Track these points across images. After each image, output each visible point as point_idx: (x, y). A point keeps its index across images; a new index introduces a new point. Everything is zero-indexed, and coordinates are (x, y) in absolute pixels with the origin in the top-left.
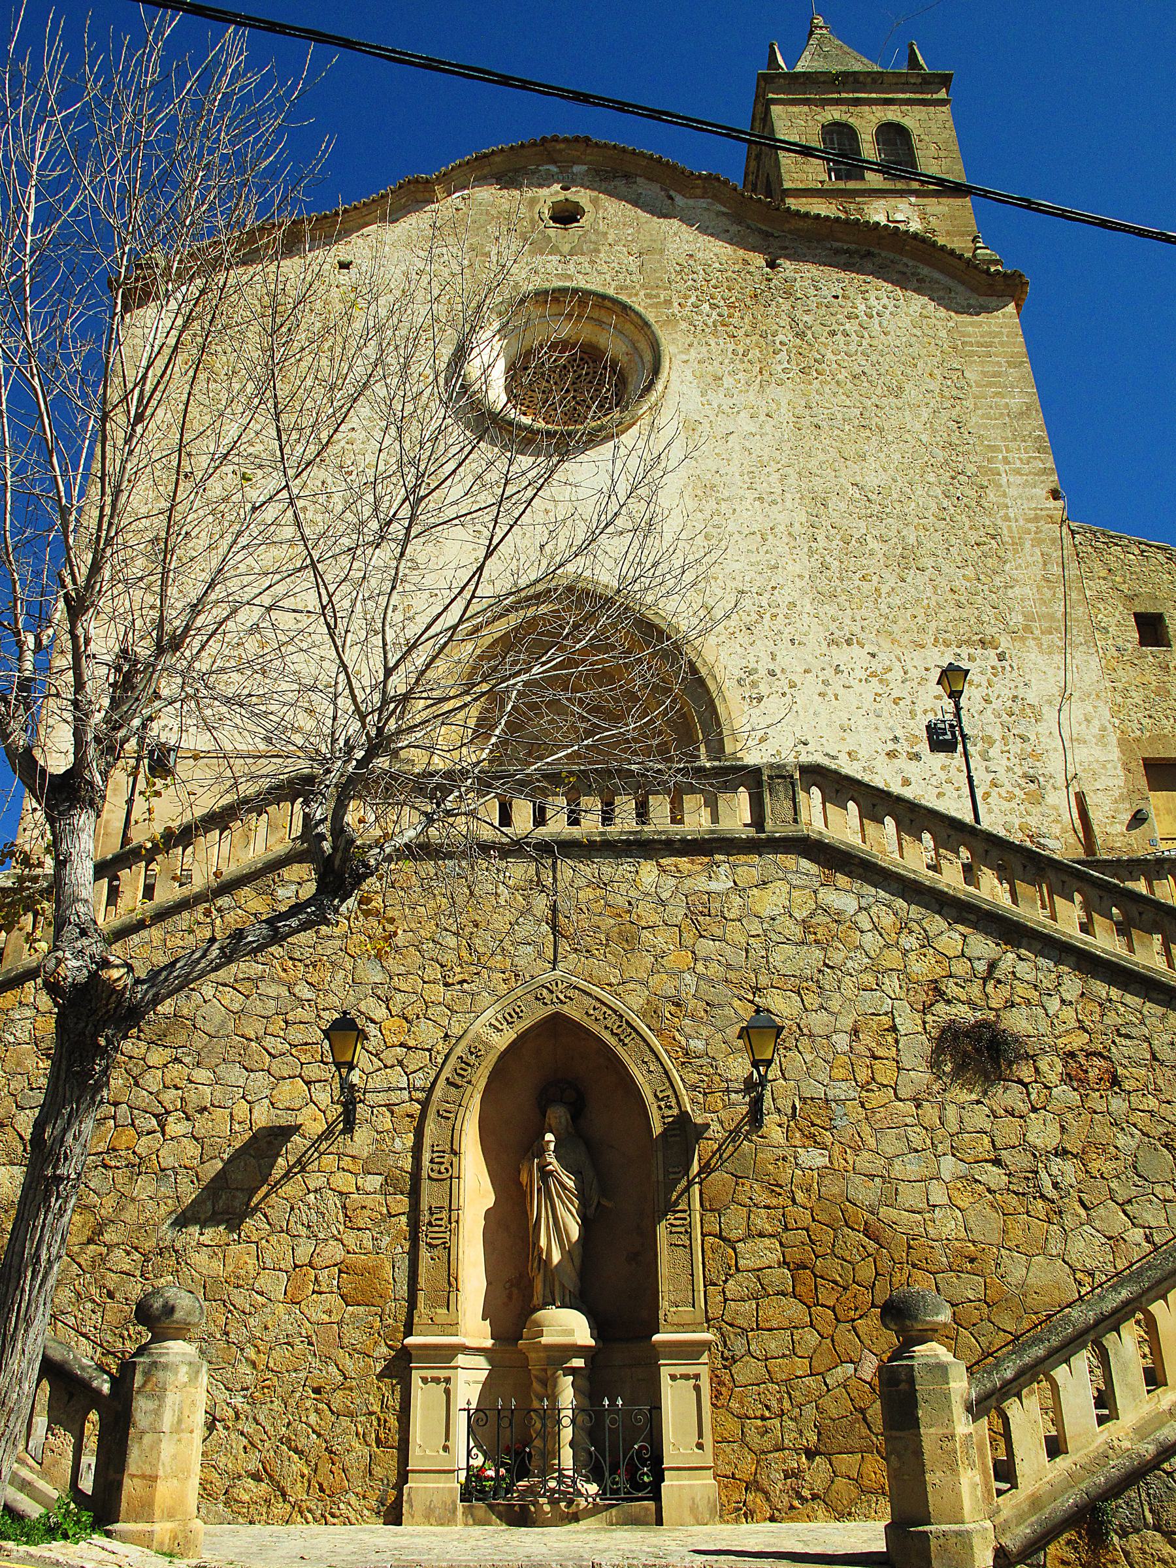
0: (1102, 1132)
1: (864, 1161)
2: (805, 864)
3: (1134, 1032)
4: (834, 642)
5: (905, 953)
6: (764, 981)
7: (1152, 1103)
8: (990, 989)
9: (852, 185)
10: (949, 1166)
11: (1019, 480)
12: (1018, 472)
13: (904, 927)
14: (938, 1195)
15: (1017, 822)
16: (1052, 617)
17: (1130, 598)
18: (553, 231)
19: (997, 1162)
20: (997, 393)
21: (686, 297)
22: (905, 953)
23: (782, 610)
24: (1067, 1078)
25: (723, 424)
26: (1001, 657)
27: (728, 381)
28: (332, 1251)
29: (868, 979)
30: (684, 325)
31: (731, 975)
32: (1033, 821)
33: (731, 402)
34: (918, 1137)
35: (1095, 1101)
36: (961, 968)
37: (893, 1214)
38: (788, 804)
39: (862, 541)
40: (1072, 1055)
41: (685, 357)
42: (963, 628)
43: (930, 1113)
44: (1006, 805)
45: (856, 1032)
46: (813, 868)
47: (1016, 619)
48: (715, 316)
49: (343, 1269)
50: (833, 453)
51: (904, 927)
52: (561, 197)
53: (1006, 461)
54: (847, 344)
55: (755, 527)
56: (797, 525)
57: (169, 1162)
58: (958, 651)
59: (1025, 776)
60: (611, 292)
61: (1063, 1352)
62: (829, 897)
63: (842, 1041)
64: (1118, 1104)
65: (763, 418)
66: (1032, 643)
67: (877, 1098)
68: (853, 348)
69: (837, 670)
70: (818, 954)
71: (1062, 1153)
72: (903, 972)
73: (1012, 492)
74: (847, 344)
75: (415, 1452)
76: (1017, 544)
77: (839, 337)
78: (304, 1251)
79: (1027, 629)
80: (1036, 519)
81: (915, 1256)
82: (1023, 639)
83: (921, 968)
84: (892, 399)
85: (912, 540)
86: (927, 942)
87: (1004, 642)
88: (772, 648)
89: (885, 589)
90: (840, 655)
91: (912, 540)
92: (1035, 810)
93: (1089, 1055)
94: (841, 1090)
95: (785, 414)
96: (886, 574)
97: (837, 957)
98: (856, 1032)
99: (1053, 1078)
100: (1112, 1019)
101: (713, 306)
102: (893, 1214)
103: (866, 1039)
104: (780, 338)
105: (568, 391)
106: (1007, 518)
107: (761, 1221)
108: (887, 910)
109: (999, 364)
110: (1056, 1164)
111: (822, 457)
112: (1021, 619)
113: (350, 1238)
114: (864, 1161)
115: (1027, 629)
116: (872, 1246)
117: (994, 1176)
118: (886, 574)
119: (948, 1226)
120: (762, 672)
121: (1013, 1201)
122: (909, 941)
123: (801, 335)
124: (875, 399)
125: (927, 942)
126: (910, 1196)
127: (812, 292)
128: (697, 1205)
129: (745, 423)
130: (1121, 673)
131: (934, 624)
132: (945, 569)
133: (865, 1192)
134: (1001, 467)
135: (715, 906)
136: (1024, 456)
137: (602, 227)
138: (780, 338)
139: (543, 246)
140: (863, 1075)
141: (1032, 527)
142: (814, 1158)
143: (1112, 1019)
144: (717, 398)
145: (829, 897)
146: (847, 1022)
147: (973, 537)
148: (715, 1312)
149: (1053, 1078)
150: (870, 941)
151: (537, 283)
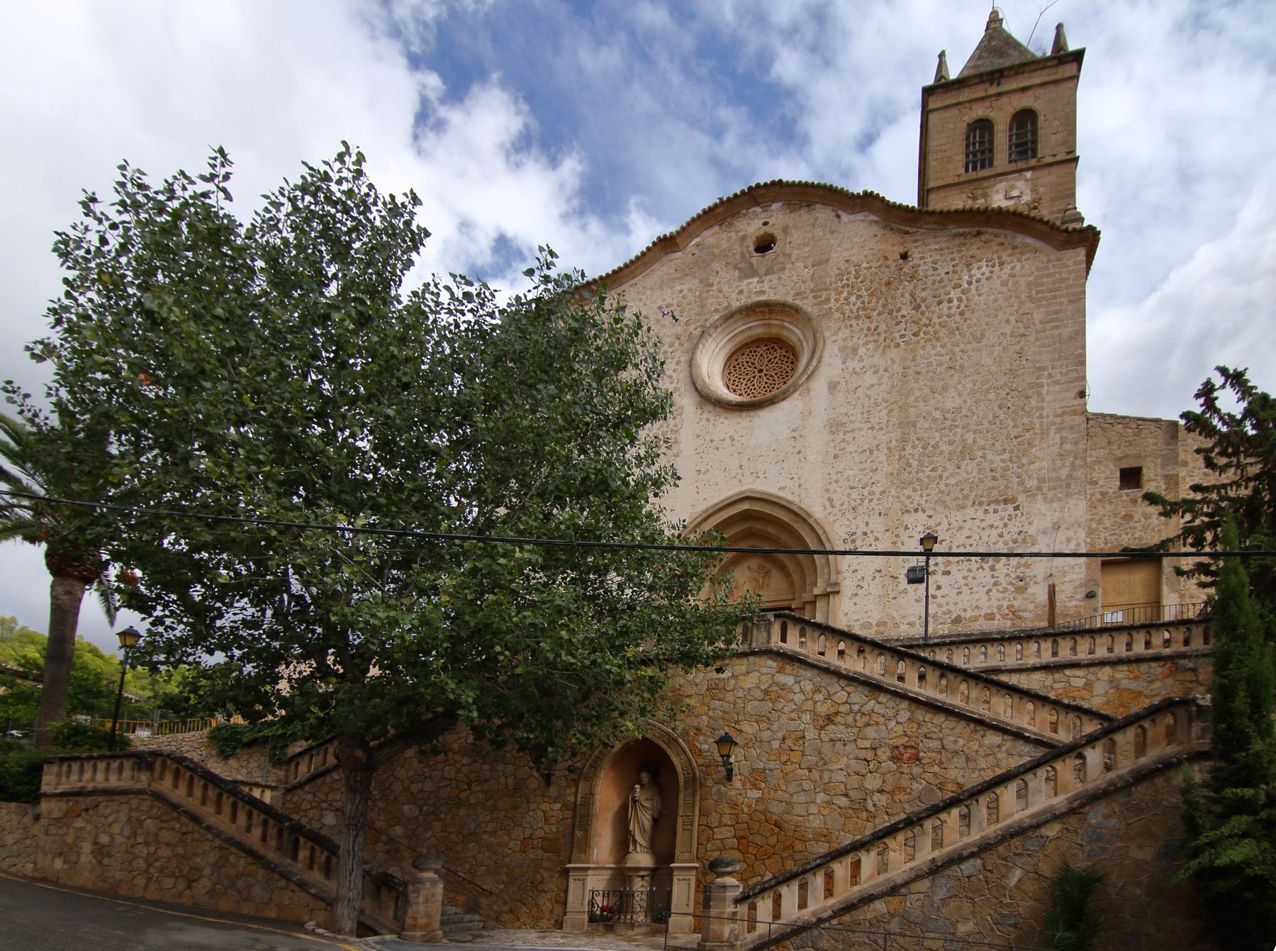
0: (905, 782)
1: (779, 795)
2: (770, 662)
3: (934, 736)
4: (908, 511)
5: (815, 703)
6: (741, 717)
7: (936, 769)
8: (858, 718)
9: (987, 172)
10: (821, 797)
11: (1056, 388)
12: (1057, 383)
13: (817, 690)
14: (813, 809)
15: (1005, 604)
16: (1058, 479)
17: (1120, 459)
18: (756, 258)
19: (846, 795)
20: (1053, 328)
21: (841, 293)
22: (815, 703)
23: (878, 495)
24: (893, 758)
25: (855, 381)
26: (1016, 508)
27: (862, 351)
28: (540, 833)
29: (794, 715)
30: (837, 315)
31: (726, 716)
32: (1016, 603)
33: (861, 365)
34: (806, 785)
35: (905, 768)
36: (843, 709)
37: (789, 817)
38: (765, 634)
39: (935, 446)
40: (897, 747)
42: (995, 493)
43: (815, 774)
44: (1001, 595)
45: (784, 739)
46: (774, 664)
47: (1032, 483)
48: (858, 304)
49: (543, 839)
50: (926, 390)
51: (817, 690)
52: (762, 232)
53: (1050, 376)
54: (950, 308)
55: (866, 447)
57: (473, 801)
59: (1017, 577)
60: (789, 299)
61: (787, 879)
62: (781, 678)
63: (776, 744)
64: (916, 770)
66: (1040, 497)
67: (789, 767)
68: (954, 310)
69: (906, 528)
70: (770, 705)
71: (881, 791)
72: (814, 712)
73: (1049, 398)
74: (950, 308)
75: (569, 905)
76: (1044, 434)
77: (945, 305)
78: (528, 832)
79: (1039, 488)
80: (1063, 414)
81: (796, 835)
82: (1034, 496)
83: (823, 709)
84: (975, 344)
85: (970, 441)
86: (829, 697)
87: (1021, 499)
88: (867, 519)
89: (945, 475)
91: (970, 441)
92: (1019, 597)
93: (906, 747)
94: (772, 765)
95: (897, 368)
96: (948, 465)
97: (779, 706)
98: (784, 739)
99: (884, 757)
100: (924, 730)
101: (859, 297)
102: (789, 817)
103: (789, 742)
104: (903, 312)
105: (970, 283)
106: (1041, 417)
107: (726, 820)
108: (808, 680)
109: (1061, 304)
110: (877, 797)
111: (917, 393)
112: (1035, 482)
113: (547, 828)
114: (779, 795)
116: (777, 830)
117: (843, 801)
118: (948, 465)
119: (817, 822)
120: (859, 533)
121: (851, 812)
122: (819, 697)
123: (917, 308)
124: (962, 346)
125: (829, 697)
126: (799, 810)
127: (930, 273)
128: (697, 813)
129: (869, 378)
130: (1100, 509)
133: (776, 809)
134: (1044, 381)
135: (721, 685)
136: (1064, 371)
137: (788, 250)
138: (903, 312)
139: (749, 272)
140: (784, 758)
141: (1058, 420)
142: (756, 794)
143: (924, 730)
144: (853, 364)
145: (781, 678)
146: (780, 735)
147: (1014, 432)
148: (701, 855)
149: (884, 757)
150: (798, 698)
151: (743, 301)
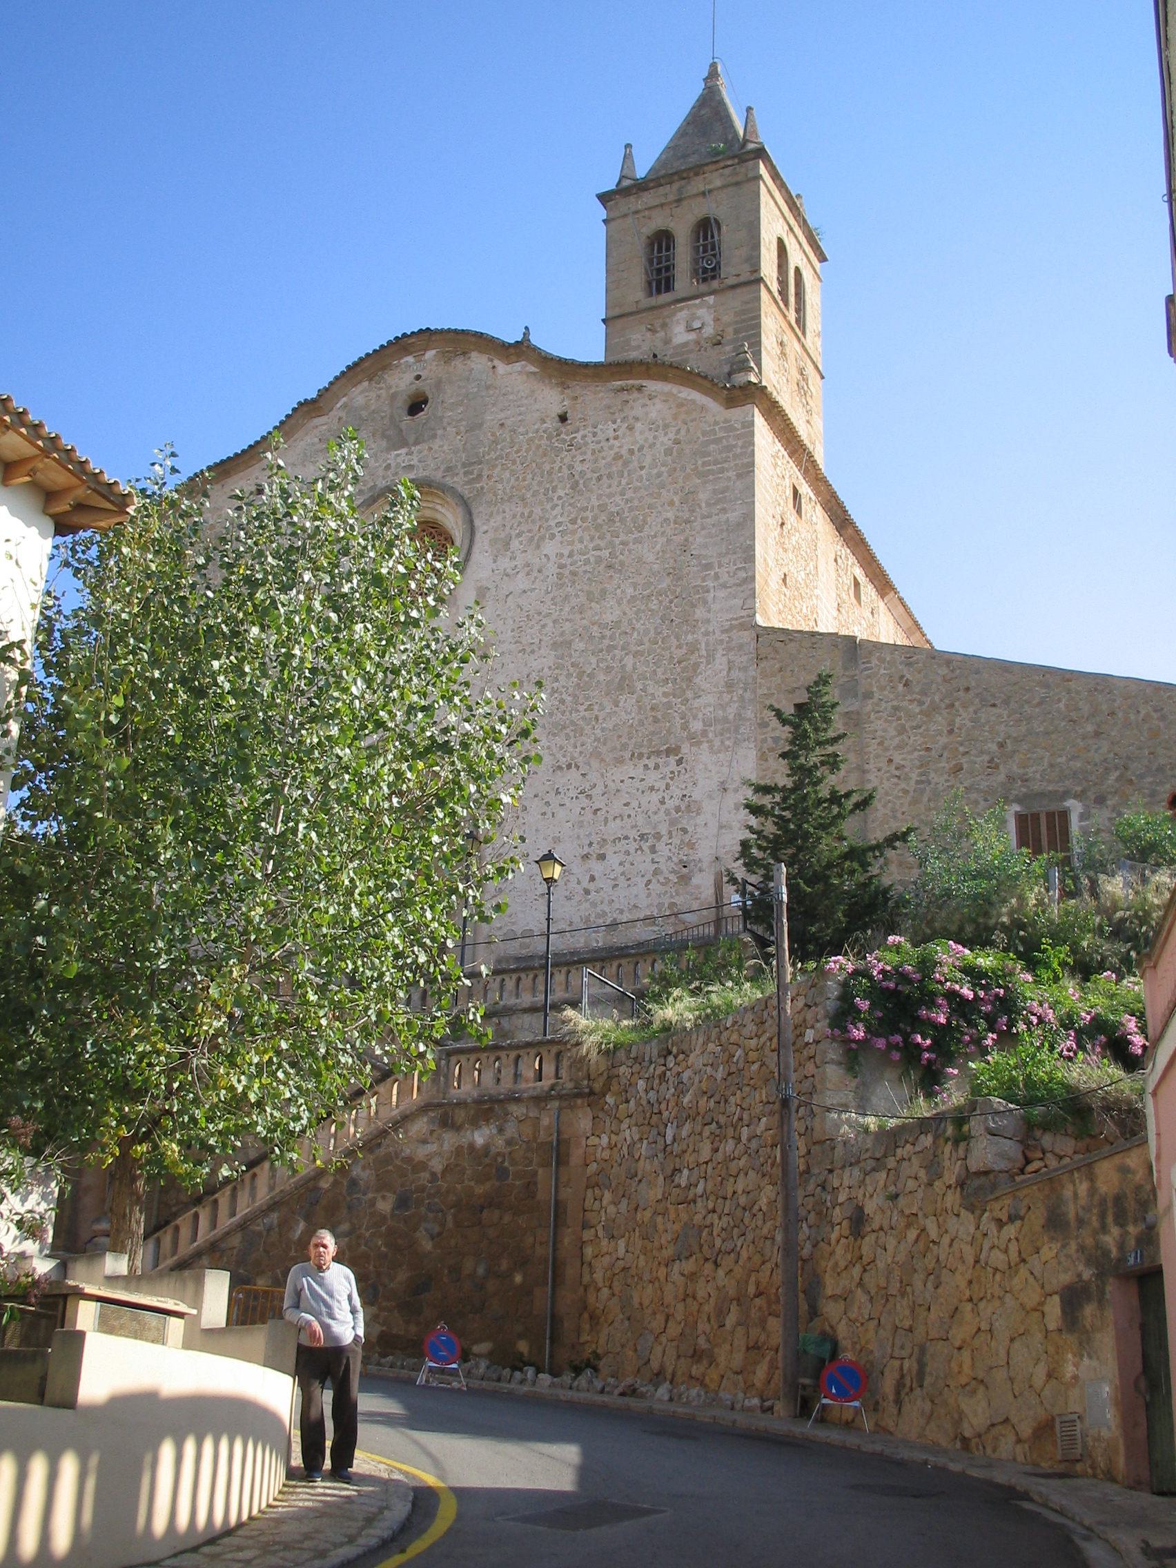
27: (515, 544)
41: (485, 528)
56: (546, 670)
58: (647, 762)
65: (535, 574)
79: (704, 733)
82: (699, 743)
90: (561, 780)
115: (704, 733)
131: (634, 740)
132: (650, 690)
139: (400, 441)
141: (724, 637)
